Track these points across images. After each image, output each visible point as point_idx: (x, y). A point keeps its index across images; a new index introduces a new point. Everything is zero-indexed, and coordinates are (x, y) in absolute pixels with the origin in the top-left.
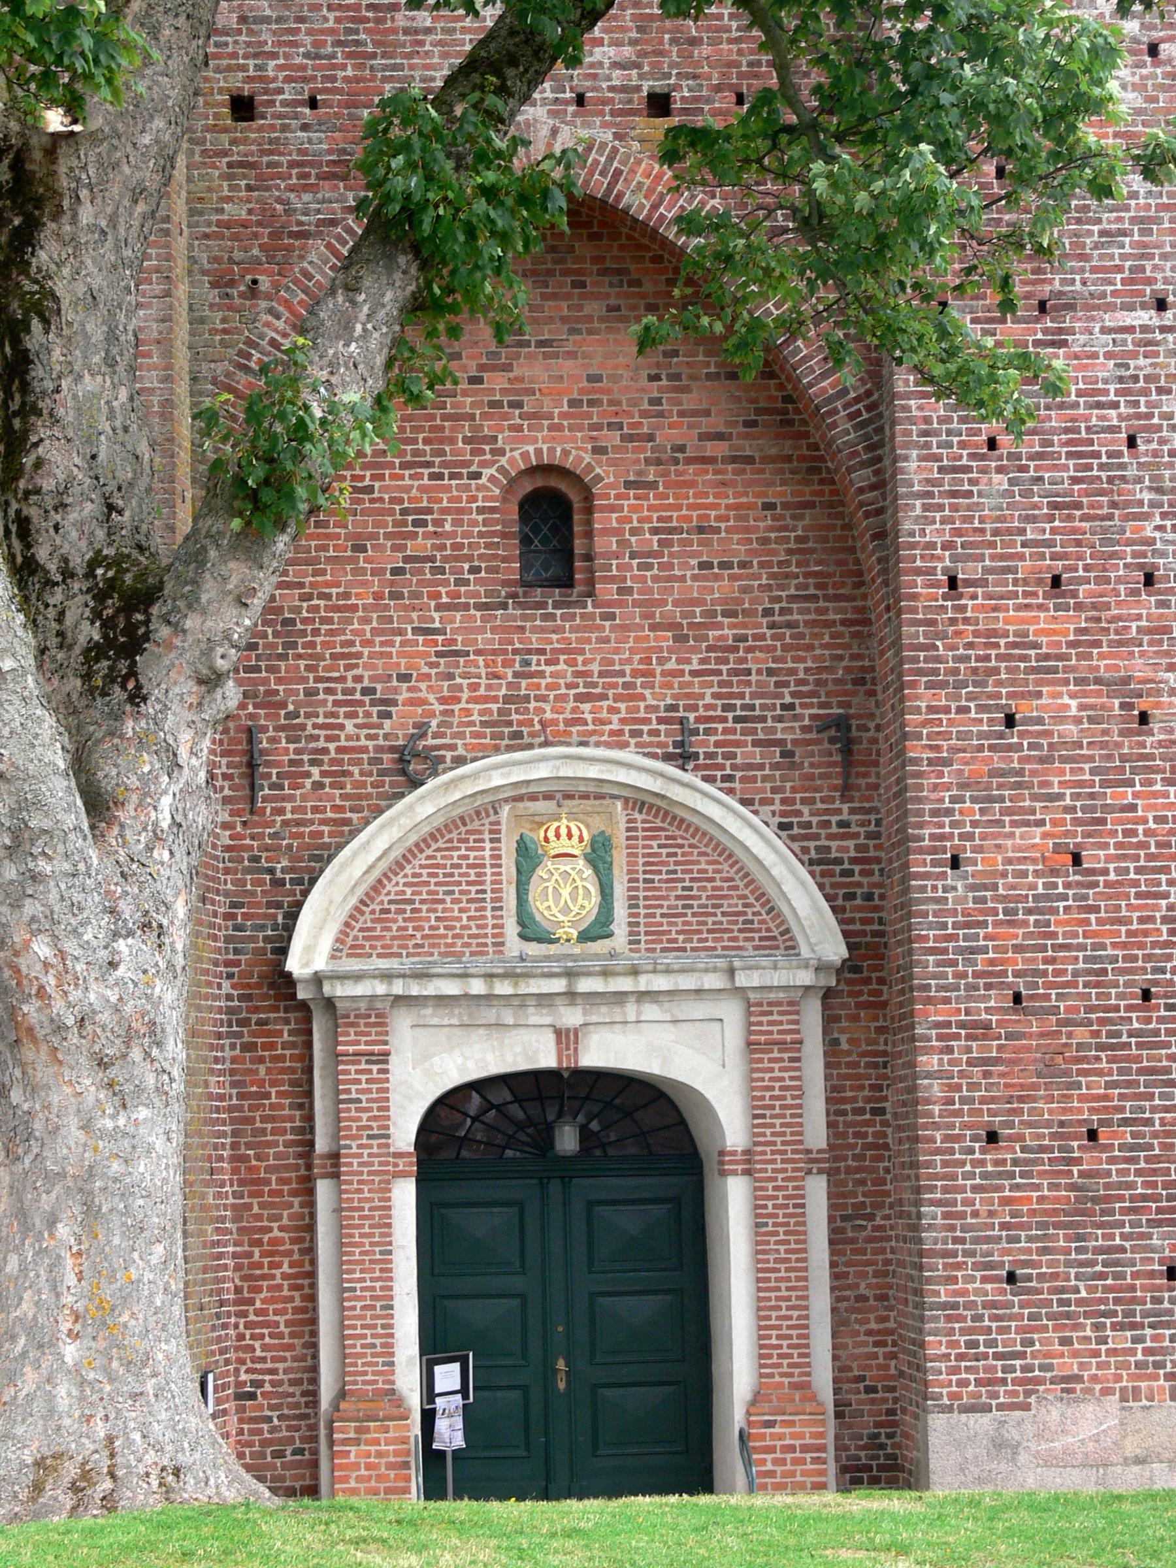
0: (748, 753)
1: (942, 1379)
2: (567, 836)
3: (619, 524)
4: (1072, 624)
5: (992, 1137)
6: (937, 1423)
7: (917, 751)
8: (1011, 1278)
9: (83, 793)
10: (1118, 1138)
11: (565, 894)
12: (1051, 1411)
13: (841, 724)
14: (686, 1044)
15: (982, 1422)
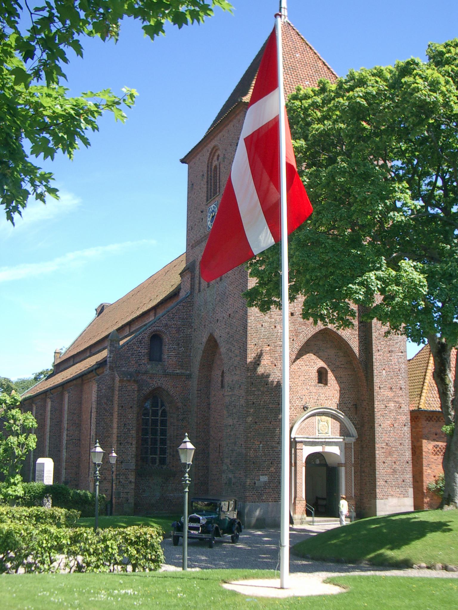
1: (378, 496)
3: (331, 376)
4: (393, 394)
5: (384, 463)
6: (377, 501)
7: (376, 410)
8: (386, 482)
9: (334, 419)
10: (398, 463)
13: (356, 405)
15: (382, 501)
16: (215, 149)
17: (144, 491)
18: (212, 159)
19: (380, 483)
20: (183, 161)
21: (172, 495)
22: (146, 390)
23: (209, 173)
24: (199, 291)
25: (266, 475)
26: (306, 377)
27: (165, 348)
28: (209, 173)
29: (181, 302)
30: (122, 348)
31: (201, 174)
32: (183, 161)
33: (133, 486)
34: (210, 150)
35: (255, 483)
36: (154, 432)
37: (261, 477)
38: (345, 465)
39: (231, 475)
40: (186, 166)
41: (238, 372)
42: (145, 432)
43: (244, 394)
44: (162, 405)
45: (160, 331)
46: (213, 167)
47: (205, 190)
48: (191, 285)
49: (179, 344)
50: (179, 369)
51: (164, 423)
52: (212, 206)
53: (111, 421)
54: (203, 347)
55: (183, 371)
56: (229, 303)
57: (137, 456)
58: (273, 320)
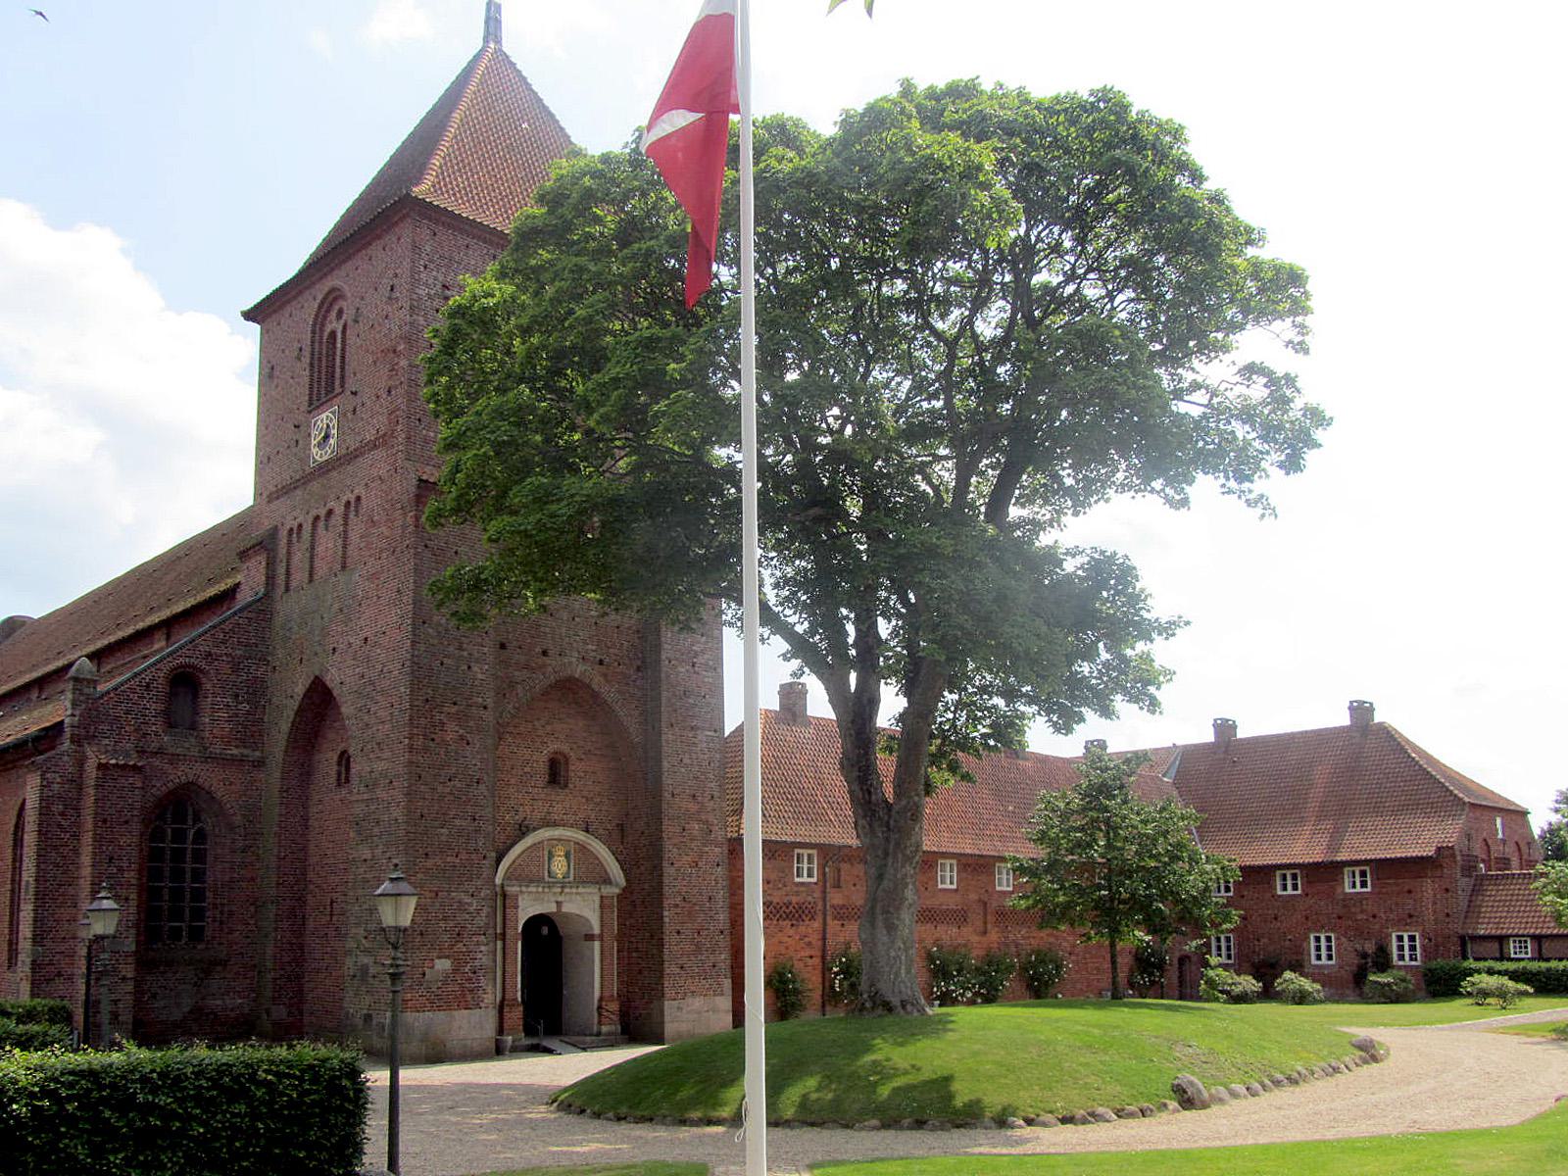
0: (601, 831)
2: (560, 851)
3: (576, 769)
5: (678, 932)
6: (666, 1003)
11: (559, 866)
12: (689, 1000)
14: (584, 907)
16: (334, 297)
17: (154, 996)
18: (325, 317)
19: (670, 969)
20: (248, 316)
21: (219, 1002)
22: (159, 788)
23: (317, 345)
24: (287, 589)
25: (447, 957)
26: (526, 770)
27: (206, 703)
28: (317, 345)
29: (241, 610)
30: (101, 697)
31: (296, 345)
32: (248, 316)
33: (130, 987)
34: (320, 297)
35: (424, 974)
36: (178, 874)
37: (437, 961)
38: (601, 937)
39: (366, 960)
40: (256, 328)
41: (387, 754)
42: (155, 874)
43: (400, 798)
44: (197, 819)
45: (193, 667)
46: (326, 334)
47: (307, 380)
48: (268, 578)
49: (237, 696)
50: (237, 747)
51: (200, 856)
52: (324, 416)
53: (76, 852)
54: (297, 704)
55: (246, 752)
56: (364, 617)
57: (137, 926)
58: (465, 654)
